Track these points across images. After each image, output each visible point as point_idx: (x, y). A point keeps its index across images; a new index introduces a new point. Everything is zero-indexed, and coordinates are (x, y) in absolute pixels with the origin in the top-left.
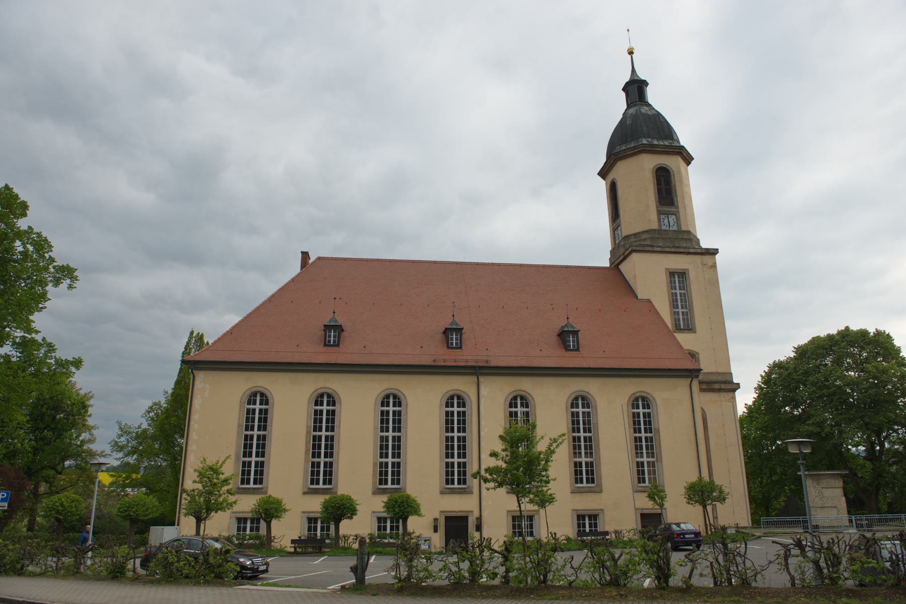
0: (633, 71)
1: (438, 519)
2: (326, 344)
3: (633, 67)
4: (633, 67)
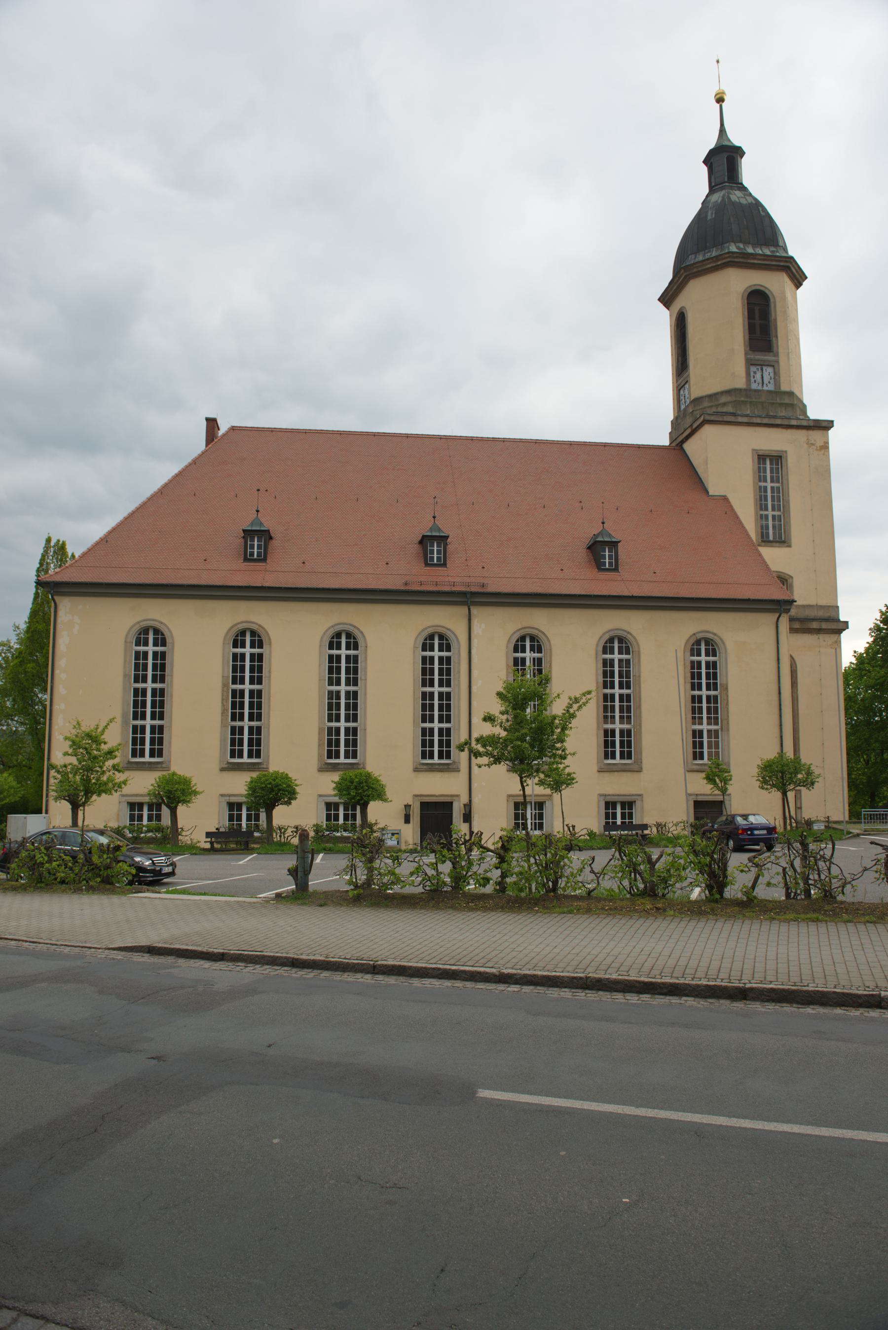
0: (722, 131)
3: (722, 124)
4: (722, 124)
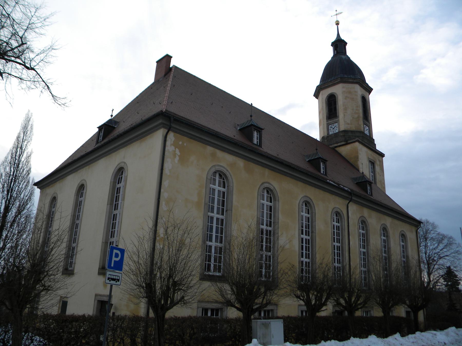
0: (338, 34)
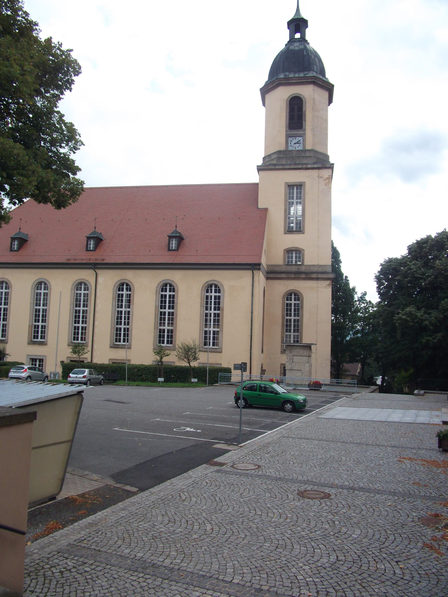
0: (298, 10)
1: (265, 370)
2: (11, 250)
3: (298, 7)
4: (298, 7)
